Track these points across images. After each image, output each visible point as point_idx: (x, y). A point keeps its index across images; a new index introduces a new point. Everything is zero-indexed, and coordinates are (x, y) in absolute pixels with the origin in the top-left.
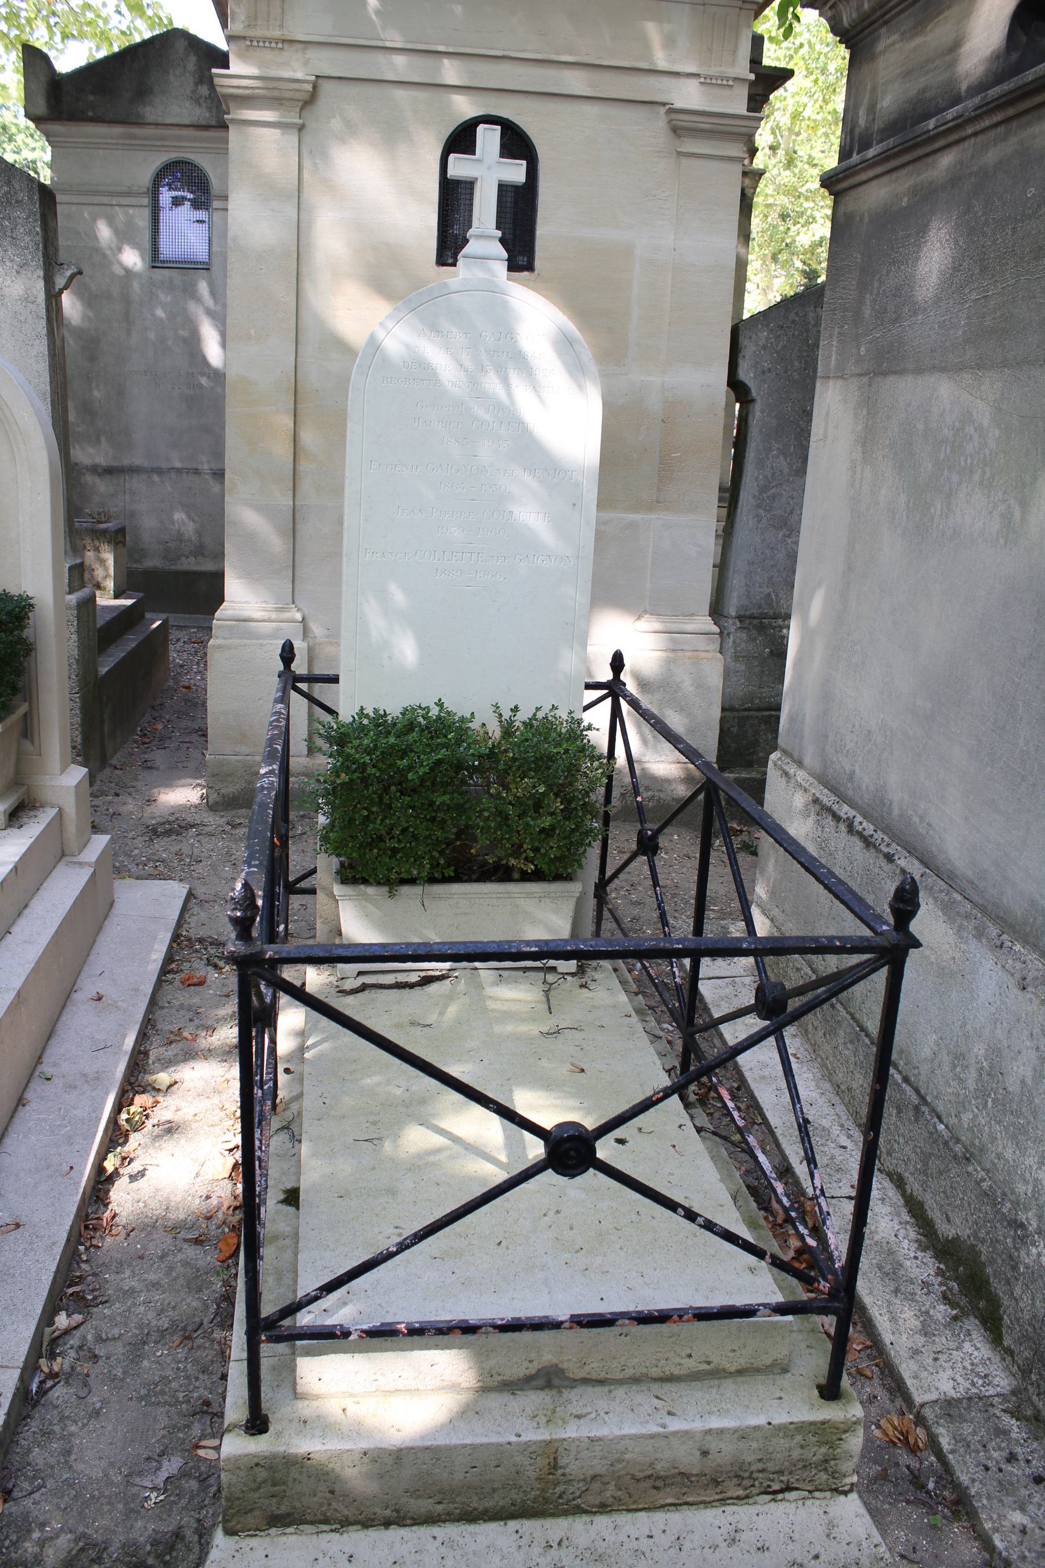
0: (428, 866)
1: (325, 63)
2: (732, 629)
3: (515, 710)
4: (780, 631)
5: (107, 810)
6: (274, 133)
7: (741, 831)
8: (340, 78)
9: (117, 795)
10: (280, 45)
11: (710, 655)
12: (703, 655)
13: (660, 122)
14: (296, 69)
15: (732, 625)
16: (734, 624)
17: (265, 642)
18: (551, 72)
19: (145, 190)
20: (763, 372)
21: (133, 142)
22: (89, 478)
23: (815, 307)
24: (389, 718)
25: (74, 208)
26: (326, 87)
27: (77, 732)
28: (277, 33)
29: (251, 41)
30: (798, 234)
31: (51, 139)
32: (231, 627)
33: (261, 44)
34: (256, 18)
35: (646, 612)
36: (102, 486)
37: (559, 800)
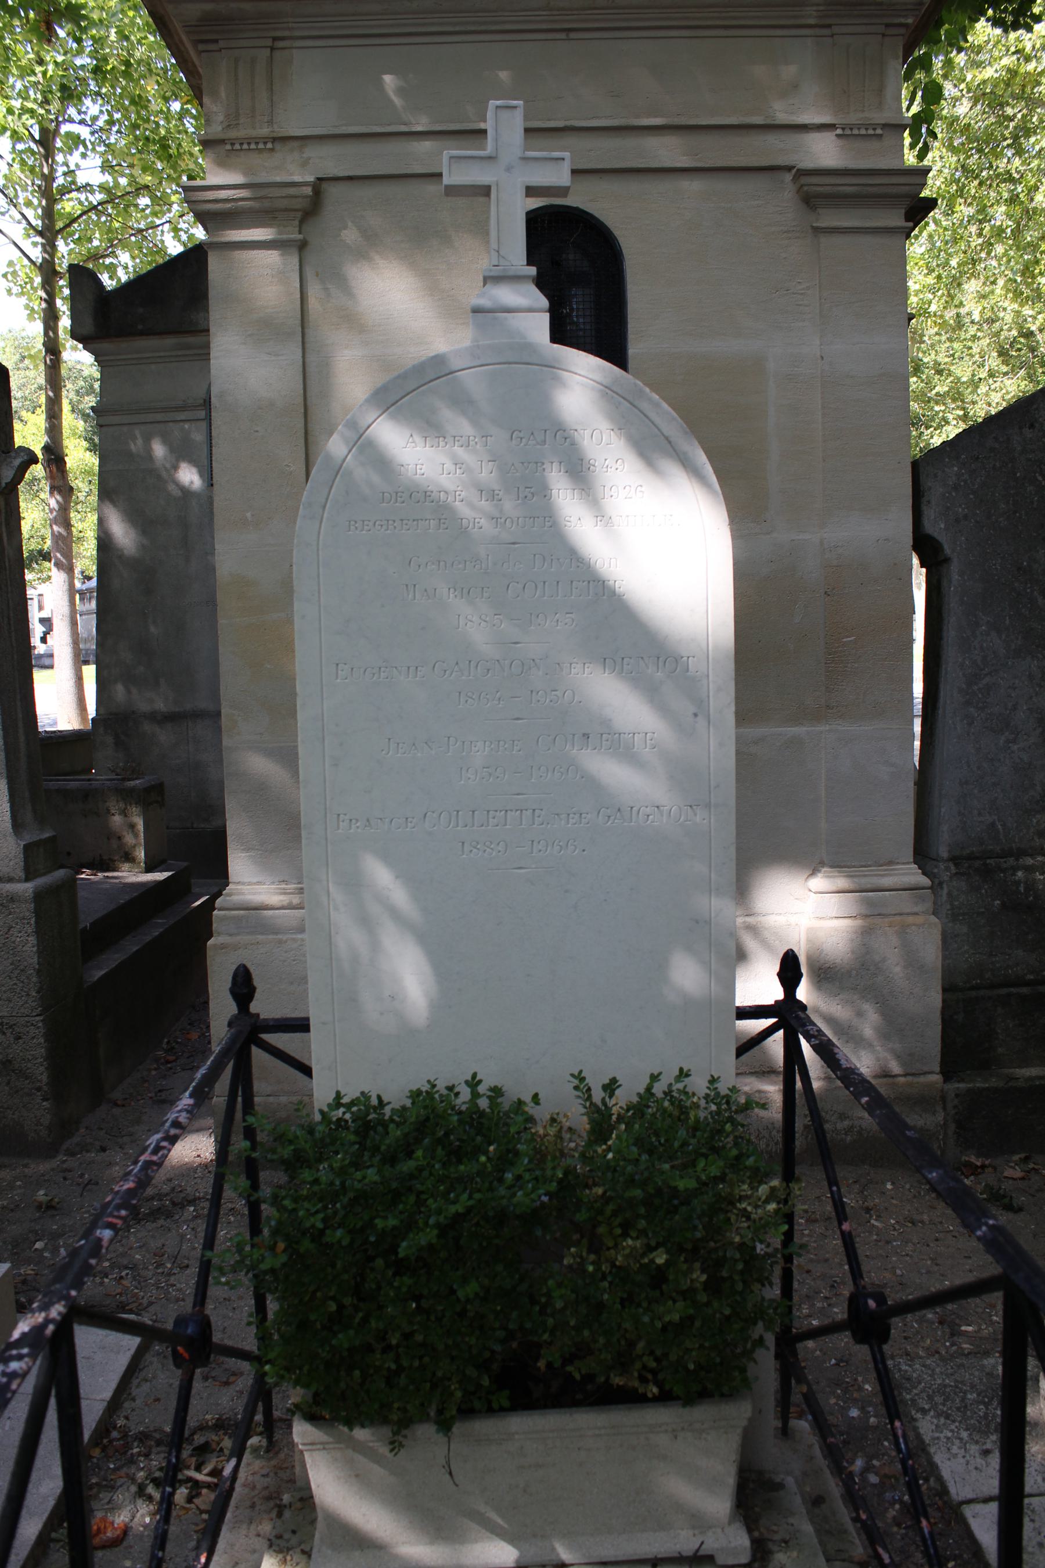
0: (459, 1394)
1: (328, 161)
2: (945, 876)
3: (611, 1087)
4: (1014, 874)
5: (82, 1176)
6: (272, 257)
7: (983, 1167)
8: (350, 178)
9: (103, 1149)
10: (269, 146)
11: (920, 919)
12: (910, 919)
13: (787, 192)
14: (296, 171)
15: (945, 871)
16: (947, 869)
17: (284, 937)
18: (630, 142)
19: (202, 401)
20: (957, 521)
21: (188, 352)
22: (147, 727)
23: (1021, 428)
24: (387, 1110)
25: (125, 429)
26: (333, 191)
27: (42, 1069)
28: (265, 131)
29: (233, 144)
30: (932, 437)
31: (100, 359)
32: (239, 919)
33: (245, 146)
34: (237, 116)
35: (822, 864)
36: (164, 736)
37: (697, 1265)
